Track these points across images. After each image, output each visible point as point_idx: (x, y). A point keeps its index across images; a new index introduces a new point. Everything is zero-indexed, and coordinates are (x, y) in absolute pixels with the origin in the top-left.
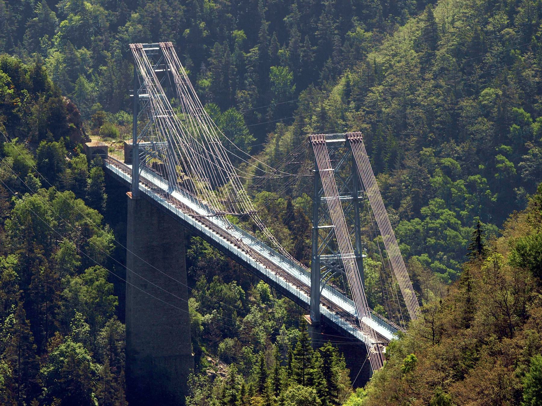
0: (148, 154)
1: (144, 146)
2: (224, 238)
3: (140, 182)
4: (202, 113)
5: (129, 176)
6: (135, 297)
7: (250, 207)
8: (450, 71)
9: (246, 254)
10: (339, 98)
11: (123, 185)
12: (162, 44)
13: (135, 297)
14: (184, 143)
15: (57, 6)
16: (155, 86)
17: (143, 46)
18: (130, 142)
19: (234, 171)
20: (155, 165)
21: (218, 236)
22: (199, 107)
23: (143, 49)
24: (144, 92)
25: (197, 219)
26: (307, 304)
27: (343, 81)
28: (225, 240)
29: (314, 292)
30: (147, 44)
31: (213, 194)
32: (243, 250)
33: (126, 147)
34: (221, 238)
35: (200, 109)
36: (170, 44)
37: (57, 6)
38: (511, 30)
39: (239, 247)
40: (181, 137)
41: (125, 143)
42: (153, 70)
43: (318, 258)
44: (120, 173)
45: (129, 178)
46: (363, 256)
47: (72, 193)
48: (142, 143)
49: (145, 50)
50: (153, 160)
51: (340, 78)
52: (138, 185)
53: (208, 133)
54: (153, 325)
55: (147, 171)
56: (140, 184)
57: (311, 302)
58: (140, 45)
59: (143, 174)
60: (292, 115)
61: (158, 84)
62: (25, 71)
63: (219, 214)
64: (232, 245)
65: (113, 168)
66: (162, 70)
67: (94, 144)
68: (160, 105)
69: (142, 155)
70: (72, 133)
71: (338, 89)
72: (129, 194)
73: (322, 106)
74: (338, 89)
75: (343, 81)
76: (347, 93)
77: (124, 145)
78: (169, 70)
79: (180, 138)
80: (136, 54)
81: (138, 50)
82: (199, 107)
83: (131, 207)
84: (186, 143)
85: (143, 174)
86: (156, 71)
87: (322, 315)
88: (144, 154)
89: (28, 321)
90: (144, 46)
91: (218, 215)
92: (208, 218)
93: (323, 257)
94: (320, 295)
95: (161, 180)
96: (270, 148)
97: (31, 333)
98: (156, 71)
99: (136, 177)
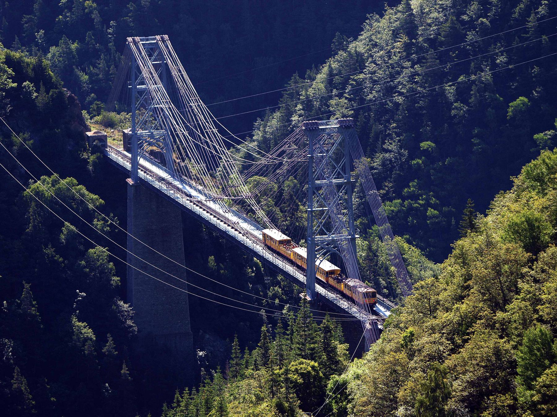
0: (146, 142)
1: (141, 135)
2: (222, 221)
3: (139, 169)
4: (198, 103)
5: (128, 164)
6: (136, 278)
7: (245, 191)
8: (428, 59)
9: (243, 236)
10: (322, 86)
11: (125, 173)
12: (158, 37)
13: (136, 278)
14: (181, 131)
15: (103, 351)
16: (153, 77)
17: (140, 39)
18: (127, 131)
19: (229, 157)
20: (152, 153)
21: (215, 219)
22: (195, 97)
23: (141, 43)
24: (143, 83)
25: (194, 204)
26: (303, 283)
27: (325, 69)
28: (222, 223)
29: (134, 162)
30: (144, 37)
31: (207, 179)
32: (240, 233)
33: (125, 135)
34: (219, 221)
35: (196, 99)
36: (166, 37)
37: (103, 351)
38: (484, 20)
39: (236, 230)
40: (178, 125)
41: (124, 132)
42: (150, 62)
43: (313, 239)
44: (120, 161)
45: (128, 166)
46: (357, 236)
47: (73, 179)
48: (140, 132)
49: (142, 44)
50: (150, 148)
51: (323, 67)
52: (137, 172)
53: (203, 121)
54: (154, 304)
55: (145, 159)
56: (139, 171)
57: (306, 281)
58: (137, 39)
59: (142, 161)
60: (278, 103)
61: (156, 76)
62: (28, 64)
63: (216, 199)
64: (229, 228)
65: (113, 156)
66: (159, 62)
67: (95, 133)
68: (157, 95)
69: (141, 143)
70: (73, 123)
71: (322, 76)
72: (130, 181)
73: (306, 94)
74: (322, 76)
75: (325, 69)
76: (330, 83)
77: (122, 134)
78: (165, 62)
79: (177, 126)
80: (133, 47)
81: (135, 43)
82: (195, 97)
83: (131, 193)
84: (183, 131)
85: (142, 161)
86: (153, 63)
87: (318, 293)
88: (142, 142)
89: (35, 302)
90: (141, 40)
91: (214, 200)
92: (205, 202)
93: (318, 237)
94: (138, 164)
95: (159, 167)
96: (258, 135)
97: (38, 313)
98: (153, 63)
99: (134, 162)
